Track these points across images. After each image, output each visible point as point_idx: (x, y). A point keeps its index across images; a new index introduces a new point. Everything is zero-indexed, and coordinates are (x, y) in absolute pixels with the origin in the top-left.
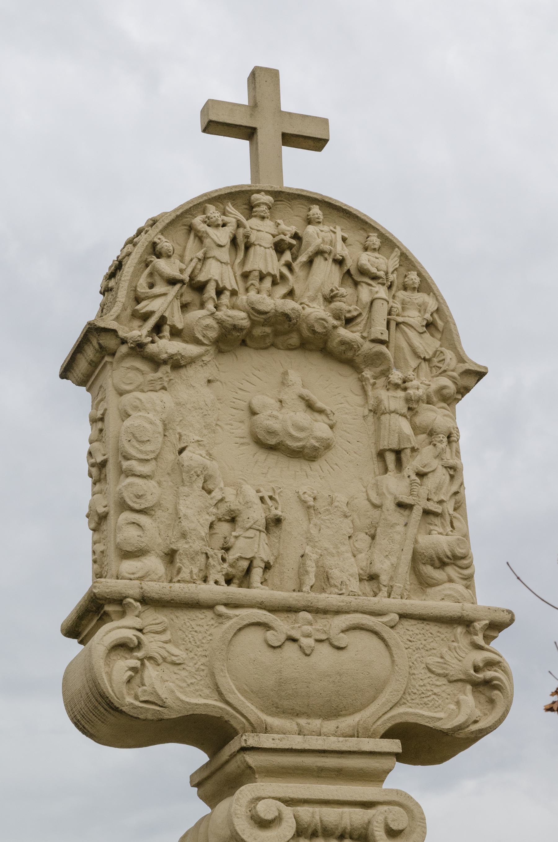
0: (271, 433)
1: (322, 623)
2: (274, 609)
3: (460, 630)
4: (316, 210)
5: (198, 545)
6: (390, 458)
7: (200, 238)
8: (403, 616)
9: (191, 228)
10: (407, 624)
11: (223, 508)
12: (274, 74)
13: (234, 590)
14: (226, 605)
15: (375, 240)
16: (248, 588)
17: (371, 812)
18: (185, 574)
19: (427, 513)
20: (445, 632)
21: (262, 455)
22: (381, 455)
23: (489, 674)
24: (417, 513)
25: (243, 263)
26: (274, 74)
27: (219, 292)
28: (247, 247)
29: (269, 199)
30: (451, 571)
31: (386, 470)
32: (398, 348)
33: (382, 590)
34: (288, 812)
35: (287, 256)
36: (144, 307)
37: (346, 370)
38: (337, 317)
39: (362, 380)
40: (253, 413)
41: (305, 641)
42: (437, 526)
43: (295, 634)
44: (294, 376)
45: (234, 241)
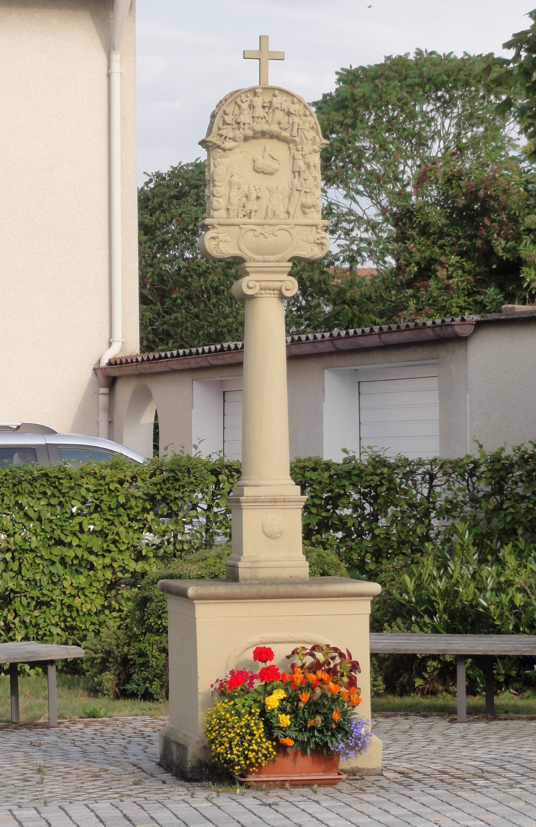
0: (259, 168)
1: (271, 228)
2: (256, 225)
3: (314, 228)
4: (277, 92)
5: (235, 207)
6: (297, 174)
7: (239, 106)
8: (296, 225)
9: (236, 103)
10: (297, 227)
11: (244, 193)
12: (267, 37)
13: (246, 220)
14: (243, 225)
15: (296, 100)
16: (291, 358)
17: (282, 283)
18: (231, 216)
19: (305, 192)
20: (309, 228)
21: (256, 174)
22: (294, 172)
23: (322, 241)
24: (303, 192)
25: (253, 112)
26: (267, 37)
27: (244, 124)
28: (254, 107)
29: (261, 90)
30: (312, 209)
31: (295, 177)
32: (301, 137)
33: (425, 223)
34: (258, 284)
35: (267, 109)
36: (221, 132)
37: (285, 144)
38: (281, 129)
39: (289, 148)
40: (254, 161)
41: (265, 234)
42: (309, 196)
43: (263, 232)
44: (268, 148)
45: (250, 106)
